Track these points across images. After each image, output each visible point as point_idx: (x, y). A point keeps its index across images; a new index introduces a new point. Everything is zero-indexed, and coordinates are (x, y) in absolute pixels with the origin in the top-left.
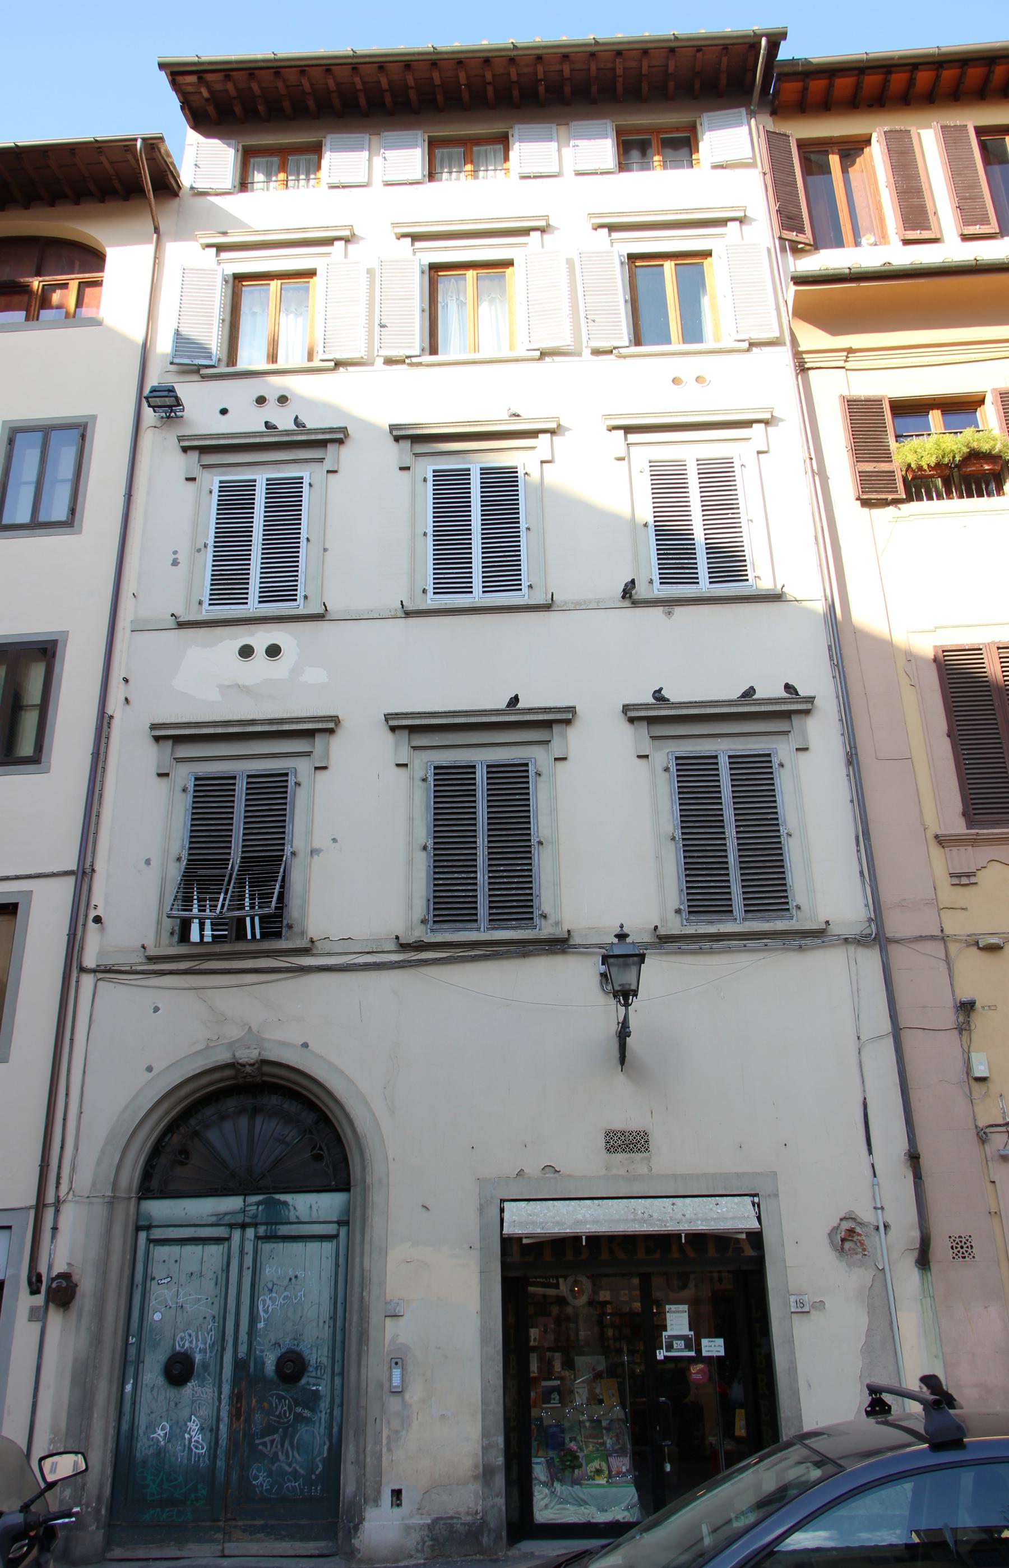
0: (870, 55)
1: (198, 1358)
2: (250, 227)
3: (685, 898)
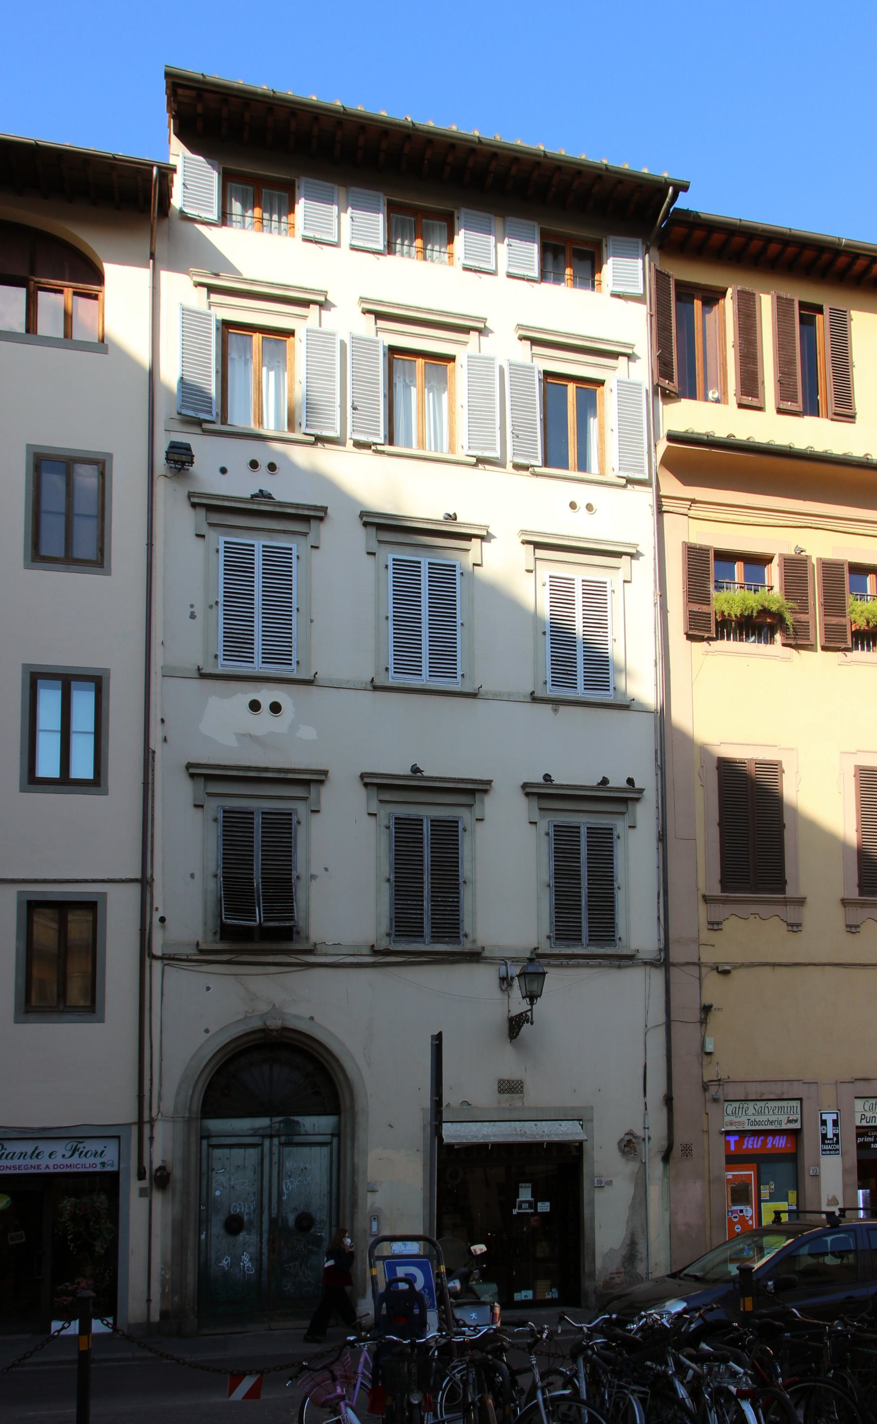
0: (743, 222)
1: (246, 1218)
2: (241, 275)
3: (554, 928)
